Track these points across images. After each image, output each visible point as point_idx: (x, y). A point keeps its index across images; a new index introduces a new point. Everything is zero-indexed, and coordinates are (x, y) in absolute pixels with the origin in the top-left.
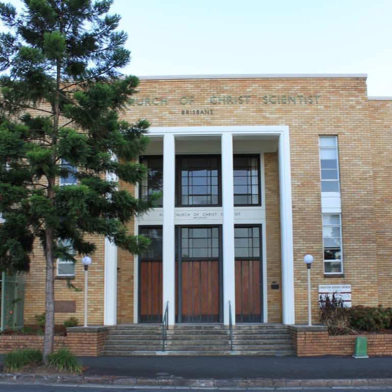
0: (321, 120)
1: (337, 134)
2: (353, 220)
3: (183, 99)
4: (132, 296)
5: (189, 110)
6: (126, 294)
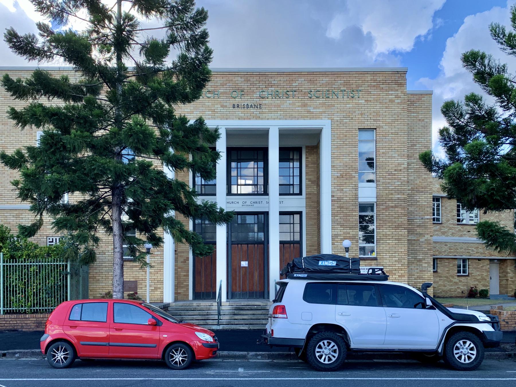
0: (362, 114)
1: (375, 127)
2: (387, 208)
3: (234, 93)
4: (188, 276)
5: (240, 104)
6: (182, 274)
